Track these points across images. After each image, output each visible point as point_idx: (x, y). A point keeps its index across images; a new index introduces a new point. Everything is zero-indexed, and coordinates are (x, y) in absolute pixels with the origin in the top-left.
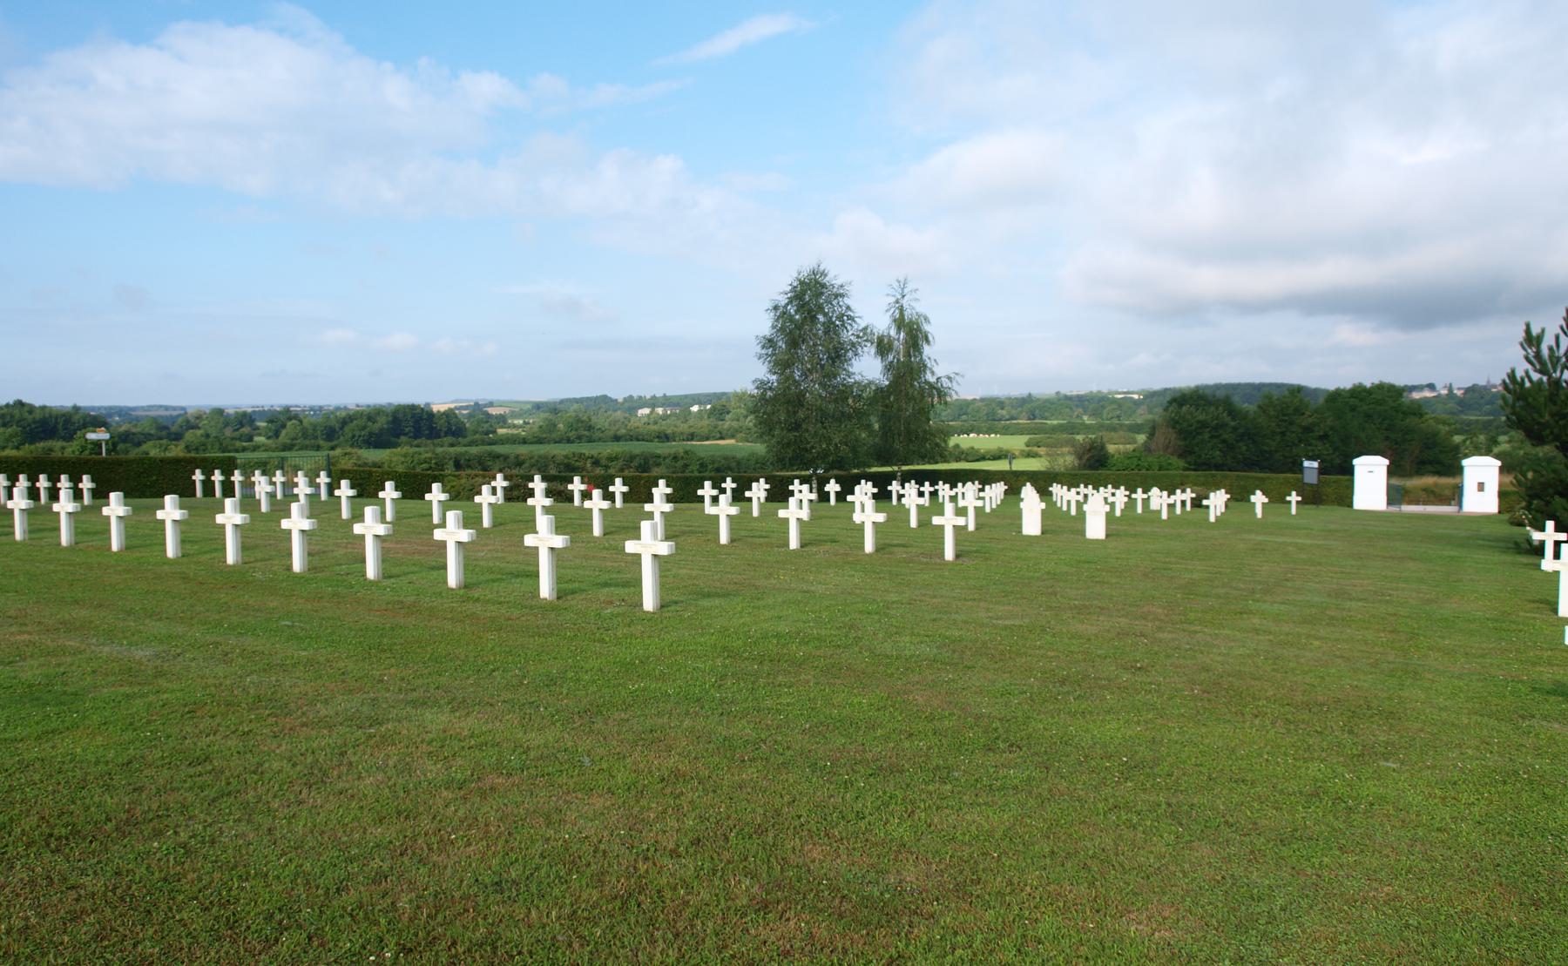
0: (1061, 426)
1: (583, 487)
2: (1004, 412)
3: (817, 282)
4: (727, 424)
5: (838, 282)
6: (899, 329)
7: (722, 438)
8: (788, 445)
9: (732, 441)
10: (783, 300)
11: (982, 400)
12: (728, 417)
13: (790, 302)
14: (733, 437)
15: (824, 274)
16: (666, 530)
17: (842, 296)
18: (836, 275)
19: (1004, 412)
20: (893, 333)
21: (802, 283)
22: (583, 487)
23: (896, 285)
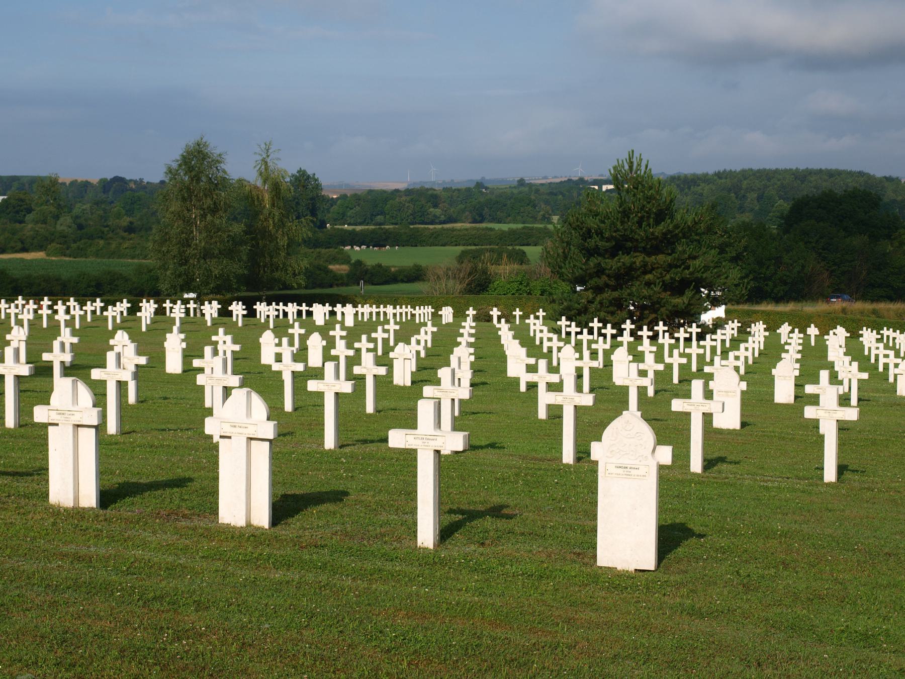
0: (512, 232)
1: (102, 305)
2: (438, 211)
3: (199, 152)
4: (29, 228)
5: (217, 152)
6: (265, 182)
7: (24, 250)
8: (180, 276)
9: (40, 255)
10: (175, 166)
11: (408, 192)
12: (29, 217)
13: (180, 165)
14: (40, 248)
15: (205, 145)
16: (27, 357)
17: (219, 162)
18: (215, 147)
19: (438, 211)
20: (259, 183)
21: (188, 152)
22: (102, 305)
23: (263, 146)
